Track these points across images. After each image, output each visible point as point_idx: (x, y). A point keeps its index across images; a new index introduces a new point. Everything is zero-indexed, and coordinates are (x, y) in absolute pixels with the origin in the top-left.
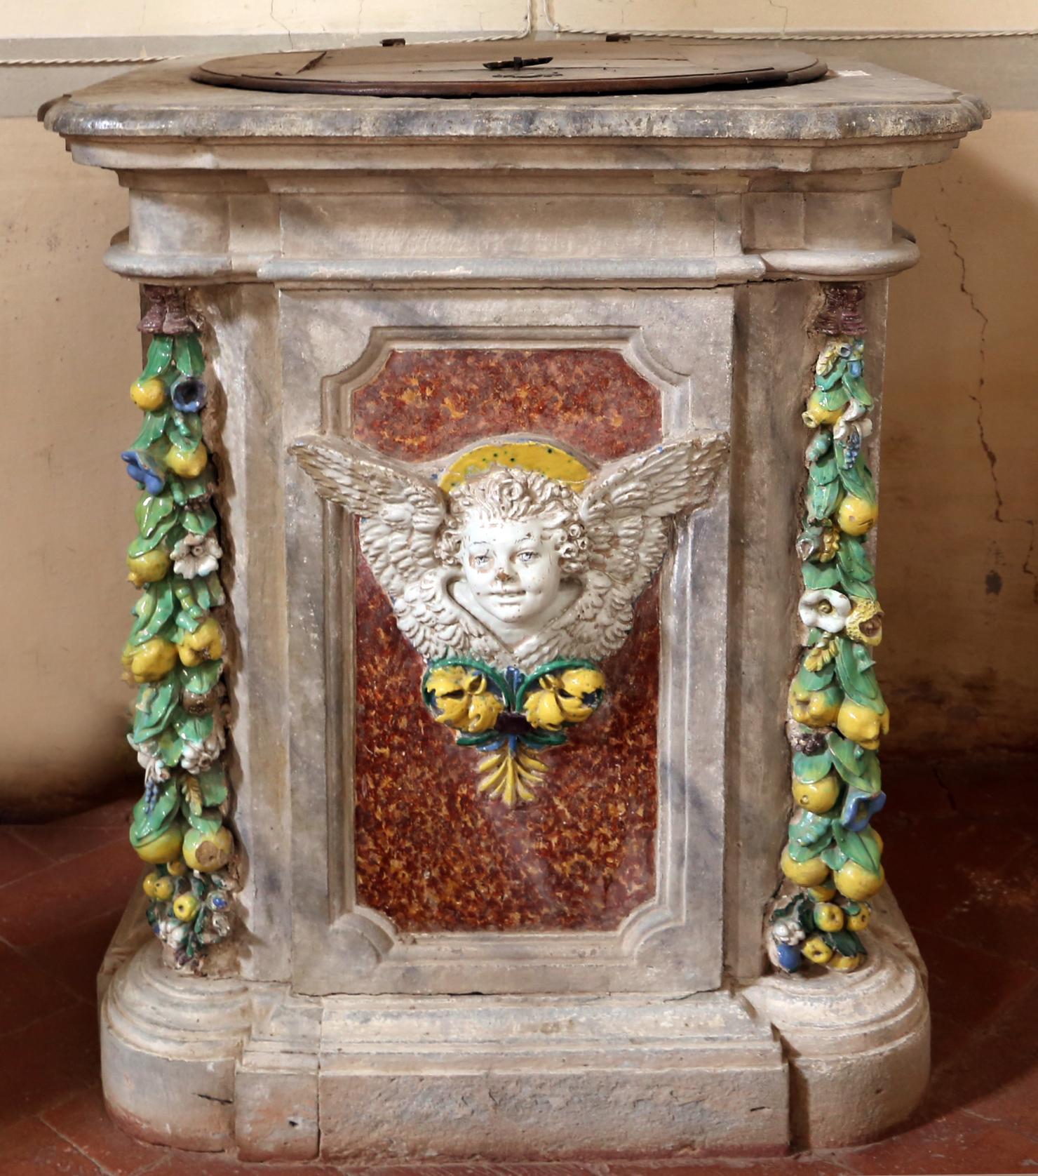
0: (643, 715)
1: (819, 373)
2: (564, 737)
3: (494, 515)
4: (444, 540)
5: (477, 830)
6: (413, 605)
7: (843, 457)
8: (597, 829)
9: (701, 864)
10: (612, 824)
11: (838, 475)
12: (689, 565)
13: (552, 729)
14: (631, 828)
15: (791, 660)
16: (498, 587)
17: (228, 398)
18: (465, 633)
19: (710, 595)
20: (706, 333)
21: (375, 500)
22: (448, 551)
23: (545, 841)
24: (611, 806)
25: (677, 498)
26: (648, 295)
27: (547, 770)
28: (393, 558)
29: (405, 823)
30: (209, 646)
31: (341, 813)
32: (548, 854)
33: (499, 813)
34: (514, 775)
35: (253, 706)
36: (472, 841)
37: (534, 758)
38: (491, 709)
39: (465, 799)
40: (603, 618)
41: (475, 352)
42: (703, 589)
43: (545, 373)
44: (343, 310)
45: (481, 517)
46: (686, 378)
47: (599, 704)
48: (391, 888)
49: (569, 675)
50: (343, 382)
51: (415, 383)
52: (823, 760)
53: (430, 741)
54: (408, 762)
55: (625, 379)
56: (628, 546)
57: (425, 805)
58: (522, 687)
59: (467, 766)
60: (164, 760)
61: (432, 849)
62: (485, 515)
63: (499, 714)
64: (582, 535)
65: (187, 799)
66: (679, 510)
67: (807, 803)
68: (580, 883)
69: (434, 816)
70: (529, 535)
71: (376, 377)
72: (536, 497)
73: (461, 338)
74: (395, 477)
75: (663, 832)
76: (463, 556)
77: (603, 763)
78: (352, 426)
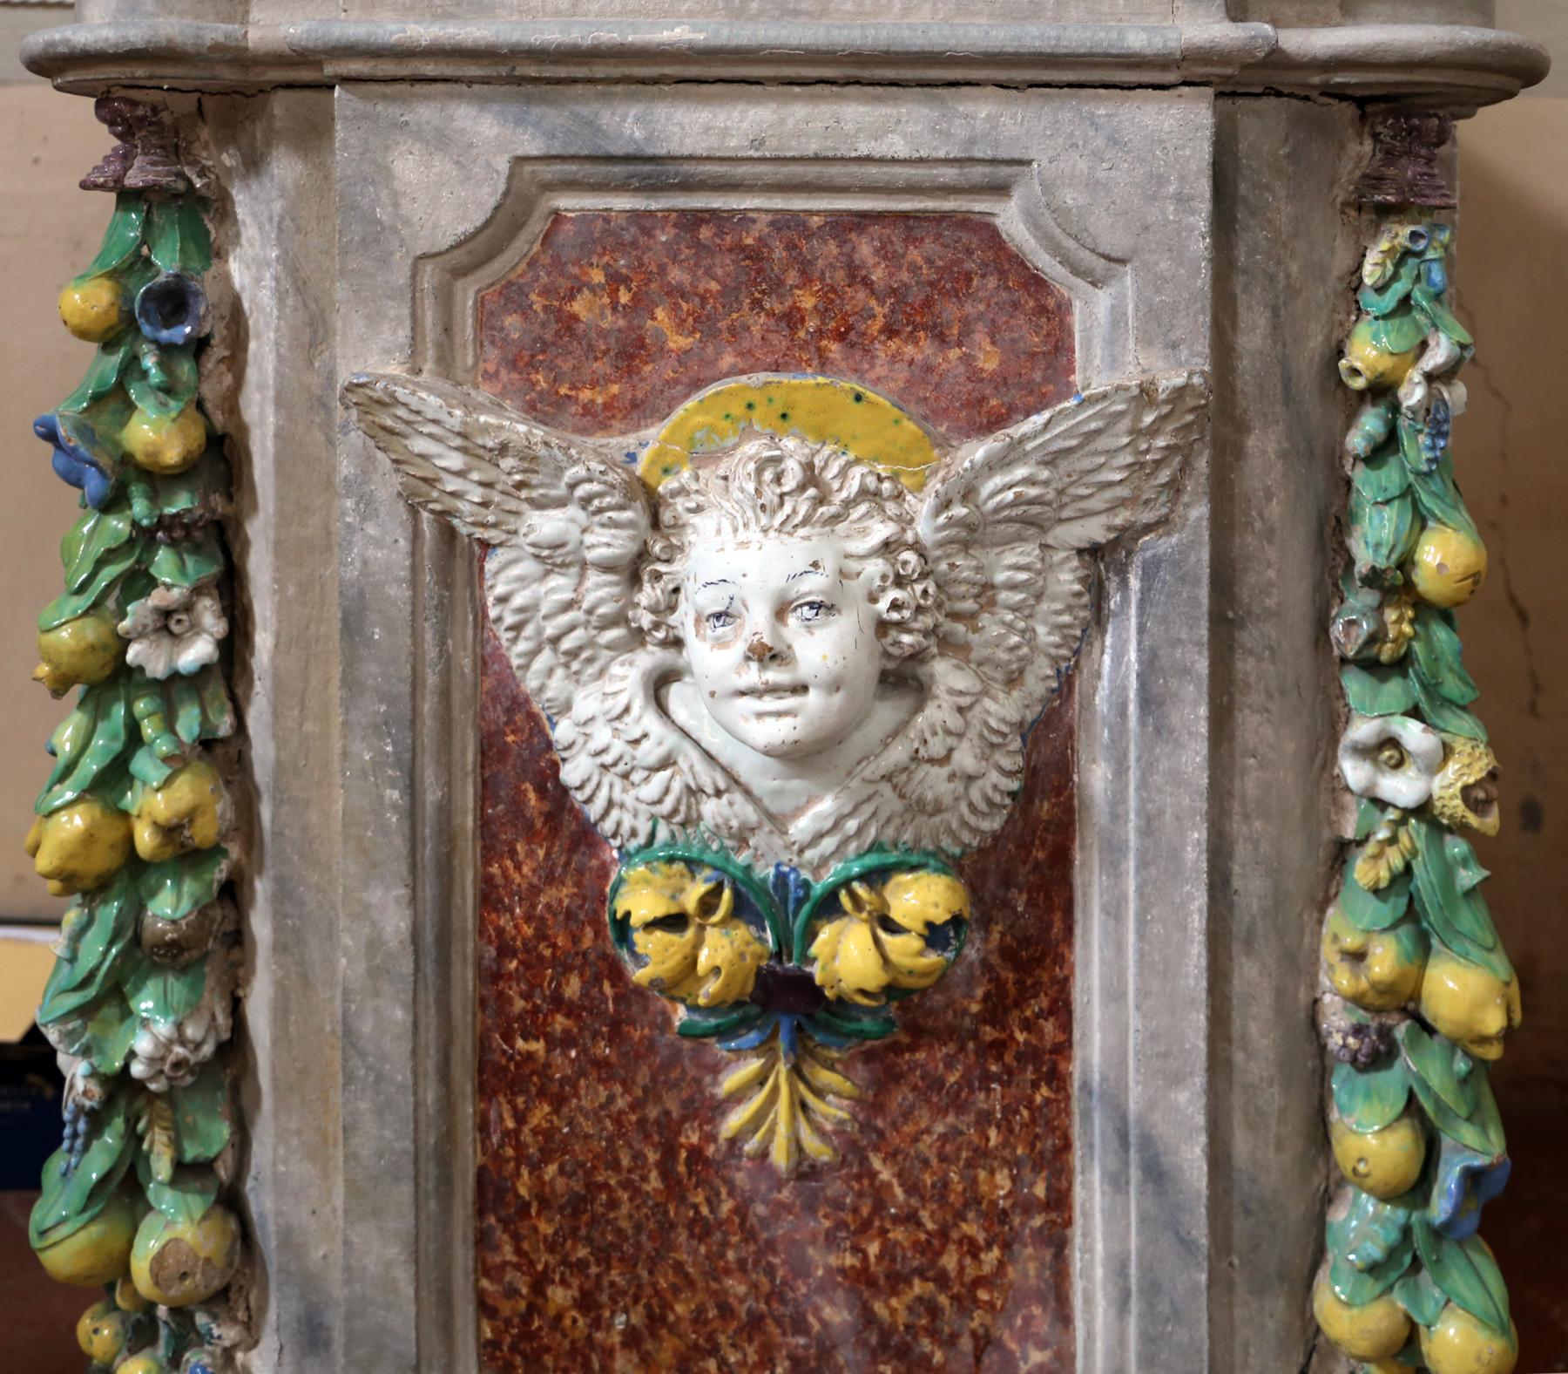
0: (1045, 977)
1: (1368, 281)
2: (889, 1022)
3: (745, 525)
4: (647, 586)
5: (720, 1224)
6: (588, 730)
7: (1417, 449)
8: (956, 1225)
9: (1164, 1307)
10: (985, 1215)
11: (1410, 486)
12: (1133, 655)
13: (865, 1001)
14: (1023, 1224)
15: (1322, 869)
16: (753, 676)
17: (251, 322)
18: (688, 787)
19: (1175, 718)
20: (1160, 176)
21: (512, 505)
22: (654, 610)
23: (856, 1249)
24: (982, 1175)
25: (1108, 510)
26: (1048, 98)
27: (856, 1093)
28: (550, 631)
29: (577, 1205)
30: (191, 815)
31: (446, 1181)
32: (861, 1280)
33: (763, 1187)
34: (792, 1104)
35: (280, 947)
36: (709, 1246)
37: (831, 1068)
38: (742, 956)
39: (696, 1153)
40: (965, 758)
41: (713, 216)
42: (1161, 705)
43: (850, 257)
44: (458, 124)
45: (719, 532)
46: (1119, 267)
47: (959, 951)
48: (548, 1350)
49: (899, 885)
50: (461, 272)
51: (598, 277)
52: (1391, 1083)
53: (626, 1028)
54: (582, 1073)
55: (1003, 275)
56: (1014, 609)
57: (615, 1165)
58: (806, 908)
59: (698, 1081)
60: (95, 1060)
61: (630, 1263)
62: (727, 526)
63: (759, 969)
64: (924, 576)
65: (145, 1146)
66: (1112, 536)
67: (1367, 1175)
68: (926, 1344)
69: (636, 1192)
70: (815, 565)
71: (523, 265)
72: (831, 492)
73: (688, 185)
74: (546, 444)
75: (1085, 1235)
76: (683, 620)
77: (966, 1081)
78: (476, 364)
